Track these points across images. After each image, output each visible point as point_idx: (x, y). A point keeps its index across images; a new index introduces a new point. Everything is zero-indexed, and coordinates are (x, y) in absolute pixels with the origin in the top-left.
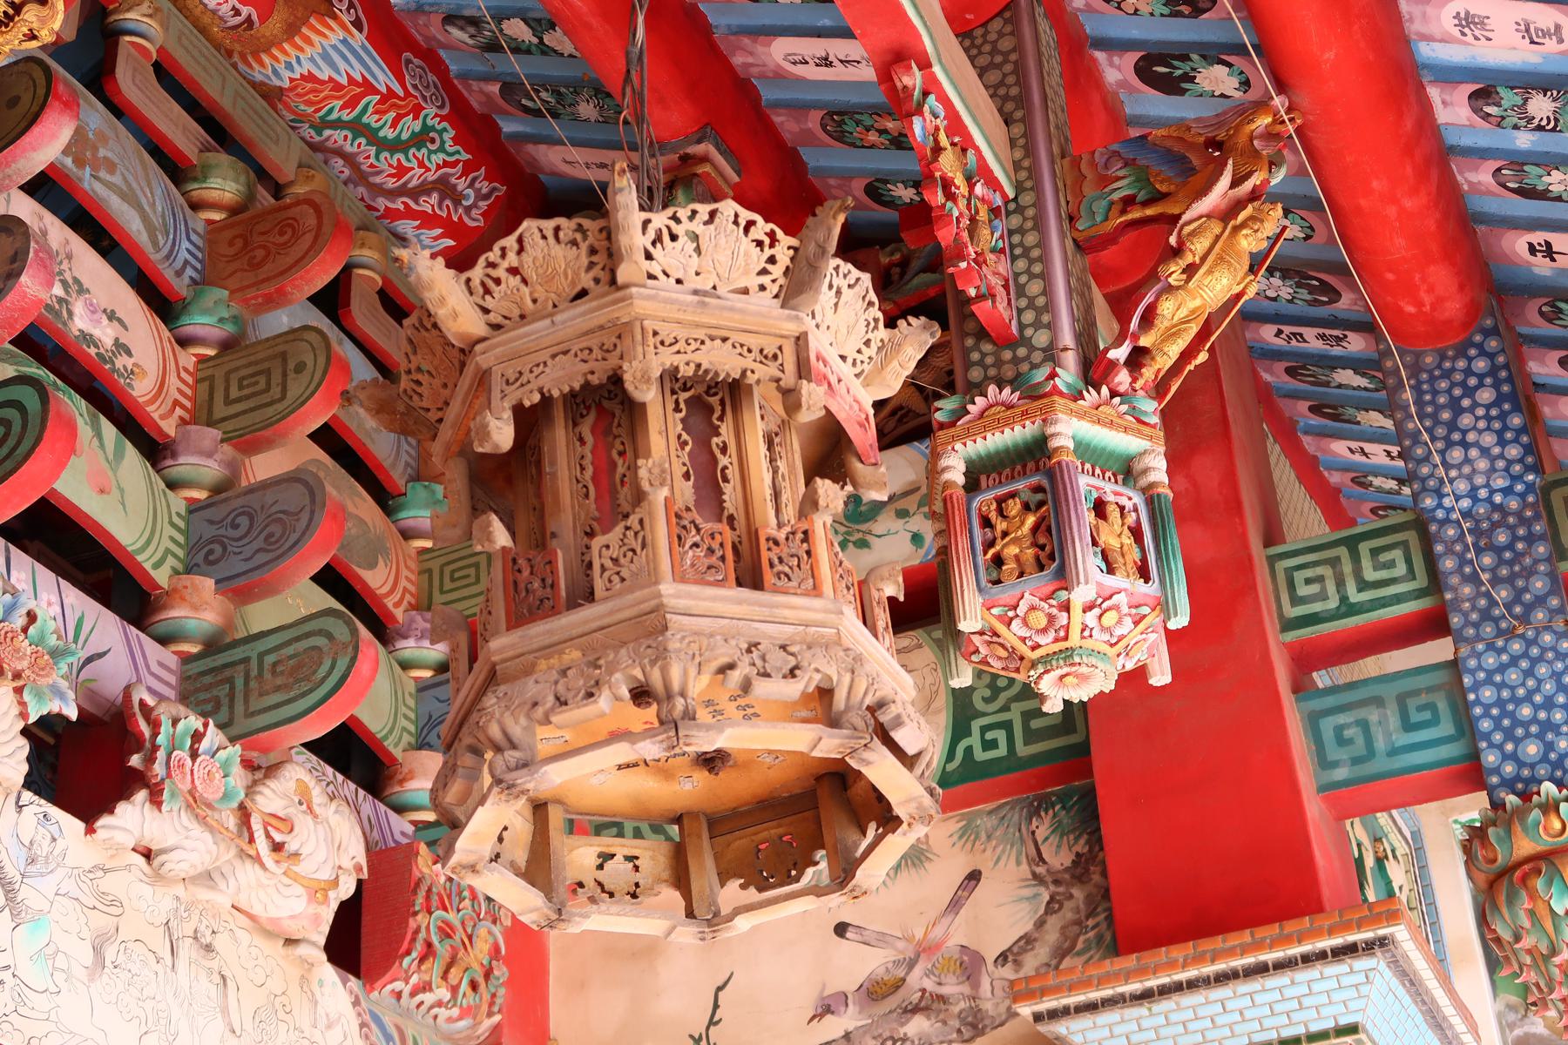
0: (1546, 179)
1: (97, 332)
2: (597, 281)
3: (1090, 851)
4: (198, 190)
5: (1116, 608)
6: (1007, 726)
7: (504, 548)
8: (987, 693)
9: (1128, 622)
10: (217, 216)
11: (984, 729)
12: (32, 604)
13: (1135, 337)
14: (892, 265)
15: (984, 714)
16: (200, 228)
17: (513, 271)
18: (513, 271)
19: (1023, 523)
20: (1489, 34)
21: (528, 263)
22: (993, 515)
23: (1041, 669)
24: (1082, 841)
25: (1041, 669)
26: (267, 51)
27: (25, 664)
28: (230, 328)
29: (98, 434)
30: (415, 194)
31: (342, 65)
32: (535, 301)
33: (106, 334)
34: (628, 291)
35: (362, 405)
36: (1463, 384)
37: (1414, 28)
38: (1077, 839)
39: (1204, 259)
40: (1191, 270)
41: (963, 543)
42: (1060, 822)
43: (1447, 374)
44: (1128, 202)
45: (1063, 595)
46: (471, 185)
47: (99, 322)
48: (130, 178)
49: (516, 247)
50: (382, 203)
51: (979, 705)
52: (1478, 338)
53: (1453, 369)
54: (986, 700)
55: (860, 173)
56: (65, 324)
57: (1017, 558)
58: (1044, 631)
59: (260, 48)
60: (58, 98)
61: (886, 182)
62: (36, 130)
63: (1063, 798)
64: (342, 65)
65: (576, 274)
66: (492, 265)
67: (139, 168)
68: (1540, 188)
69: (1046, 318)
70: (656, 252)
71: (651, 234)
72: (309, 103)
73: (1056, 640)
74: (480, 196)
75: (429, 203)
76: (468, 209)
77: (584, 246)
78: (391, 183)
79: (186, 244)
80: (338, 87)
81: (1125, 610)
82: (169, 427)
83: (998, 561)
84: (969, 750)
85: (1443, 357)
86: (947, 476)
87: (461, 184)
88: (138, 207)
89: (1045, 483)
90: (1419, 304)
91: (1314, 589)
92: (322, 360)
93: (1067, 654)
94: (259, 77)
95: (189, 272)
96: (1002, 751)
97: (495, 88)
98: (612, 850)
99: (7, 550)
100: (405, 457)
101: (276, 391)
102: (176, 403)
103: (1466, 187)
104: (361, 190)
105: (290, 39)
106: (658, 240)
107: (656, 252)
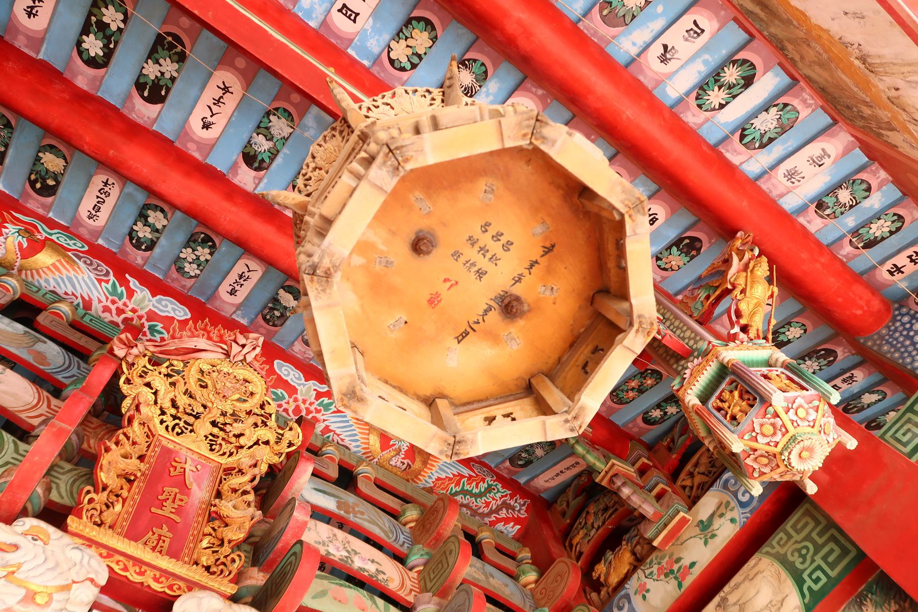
0: (871, 232)
1: (367, 567)
3: (900, 606)
4: (403, 519)
5: (800, 406)
6: (819, 568)
8: (801, 560)
9: (812, 411)
10: (412, 524)
11: (810, 576)
13: (738, 322)
14: (668, 444)
15: (805, 569)
16: (408, 530)
17: (315, 169)
18: (315, 169)
19: (733, 397)
20: (801, 175)
21: (319, 162)
22: (720, 404)
23: (786, 454)
24: (893, 604)
25: (786, 454)
26: (420, 474)
28: (426, 557)
29: (375, 603)
30: (497, 511)
31: (448, 471)
33: (371, 568)
36: (905, 329)
37: (774, 194)
38: (889, 604)
39: (746, 285)
40: (743, 291)
41: (713, 420)
42: (875, 601)
43: (896, 330)
44: (708, 297)
45: (770, 409)
46: (516, 502)
50: (487, 520)
51: (801, 567)
52: (897, 313)
53: (896, 328)
54: (802, 563)
55: (638, 415)
57: (741, 411)
58: (774, 434)
59: (418, 474)
60: (302, 457)
61: (647, 413)
63: (869, 590)
64: (448, 471)
68: (872, 238)
69: (698, 338)
70: (370, 114)
72: (443, 489)
73: (783, 435)
74: (521, 505)
75: (503, 513)
76: (519, 511)
77: (337, 134)
78: (486, 510)
79: (402, 536)
80: (450, 479)
81: (806, 406)
82: (410, 599)
83: (734, 418)
84: (809, 588)
85: (889, 327)
86: (691, 404)
87: (512, 502)
88: (378, 525)
89: (733, 377)
90: (861, 308)
91: (909, 435)
92: (457, 544)
93: (793, 439)
94: (422, 486)
95: (406, 545)
96: (824, 580)
97: (508, 464)
98: (492, 414)
100: (528, 604)
101: (445, 566)
102: (411, 590)
103: (845, 260)
104: (477, 518)
105: (426, 467)
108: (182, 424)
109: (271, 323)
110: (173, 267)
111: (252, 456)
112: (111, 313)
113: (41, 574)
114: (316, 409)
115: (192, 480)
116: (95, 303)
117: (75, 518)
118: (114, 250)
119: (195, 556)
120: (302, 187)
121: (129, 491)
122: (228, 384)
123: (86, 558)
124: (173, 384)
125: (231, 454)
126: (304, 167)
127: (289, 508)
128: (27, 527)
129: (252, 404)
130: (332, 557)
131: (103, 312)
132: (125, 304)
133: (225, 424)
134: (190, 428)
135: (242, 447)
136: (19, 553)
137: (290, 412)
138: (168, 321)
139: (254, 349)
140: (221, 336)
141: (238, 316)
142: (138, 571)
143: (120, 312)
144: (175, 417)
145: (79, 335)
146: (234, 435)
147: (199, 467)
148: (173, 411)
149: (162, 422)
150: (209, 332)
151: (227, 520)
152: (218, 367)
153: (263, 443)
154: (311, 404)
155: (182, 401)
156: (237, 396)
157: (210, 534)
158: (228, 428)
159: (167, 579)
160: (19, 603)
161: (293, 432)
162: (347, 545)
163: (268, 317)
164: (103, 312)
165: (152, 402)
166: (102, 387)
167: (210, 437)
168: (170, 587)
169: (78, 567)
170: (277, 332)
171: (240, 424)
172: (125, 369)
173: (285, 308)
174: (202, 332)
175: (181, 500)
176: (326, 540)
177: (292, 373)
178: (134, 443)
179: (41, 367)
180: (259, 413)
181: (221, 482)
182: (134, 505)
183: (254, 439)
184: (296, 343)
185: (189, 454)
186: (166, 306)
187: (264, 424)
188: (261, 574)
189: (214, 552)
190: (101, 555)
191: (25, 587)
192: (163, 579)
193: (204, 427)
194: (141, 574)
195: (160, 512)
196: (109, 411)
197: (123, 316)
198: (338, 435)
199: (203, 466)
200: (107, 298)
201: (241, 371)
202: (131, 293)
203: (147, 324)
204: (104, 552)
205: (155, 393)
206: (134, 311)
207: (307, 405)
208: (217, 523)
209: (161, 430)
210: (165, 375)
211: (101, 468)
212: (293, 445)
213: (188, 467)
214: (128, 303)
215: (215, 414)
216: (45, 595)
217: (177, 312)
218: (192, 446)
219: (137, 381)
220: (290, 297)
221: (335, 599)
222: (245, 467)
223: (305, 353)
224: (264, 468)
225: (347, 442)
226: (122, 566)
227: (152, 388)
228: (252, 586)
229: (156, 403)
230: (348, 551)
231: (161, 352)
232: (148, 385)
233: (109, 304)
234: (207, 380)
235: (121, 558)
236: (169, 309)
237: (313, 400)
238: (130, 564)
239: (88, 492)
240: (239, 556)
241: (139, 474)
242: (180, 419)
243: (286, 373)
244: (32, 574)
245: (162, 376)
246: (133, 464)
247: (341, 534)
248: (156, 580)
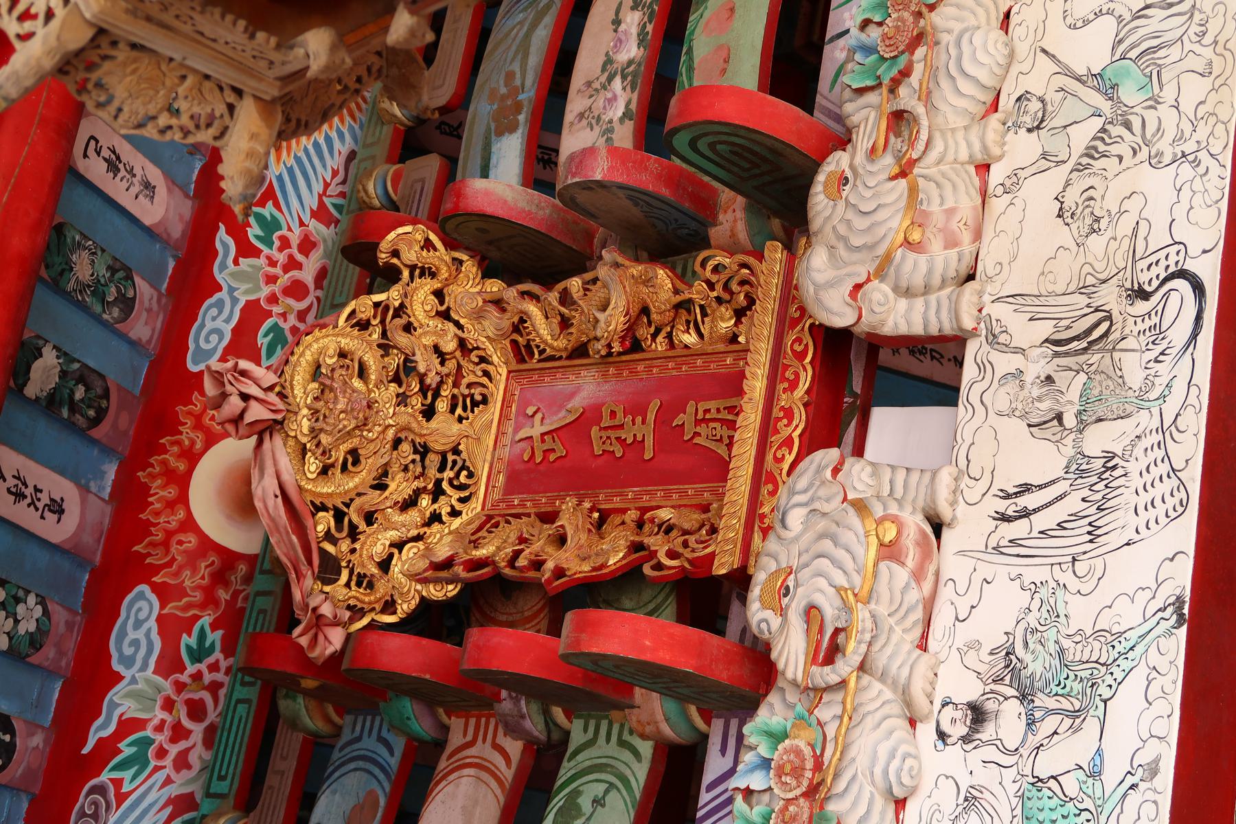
1: (634, 31)
2: (114, 44)
7: (412, 13)
12: (854, 32)
27: (906, 14)
32: (184, 77)
34: (94, 21)
35: (420, 100)
47: (625, 32)
48: (511, 54)
49: (150, 126)
56: (639, 65)
60: (457, 207)
62: (489, 210)
65: (125, 64)
66: (186, 133)
67: (500, 50)
70: (39, 8)
71: (28, 26)
77: (94, 76)
88: (528, 36)
99: (832, 40)
106: (26, 16)
107: (39, 8)
108: (449, 474)
109: (104, 404)
110: (35, 659)
111: (478, 315)
112: (188, 750)
113: (848, 551)
114: (281, 250)
115: (563, 413)
116: (174, 790)
117: (716, 563)
118: (25, 806)
119: (721, 347)
120: (212, 131)
121: (624, 511)
122: (340, 406)
123: (798, 499)
124: (369, 518)
125: (483, 360)
126: (168, 136)
127: (582, 197)
128: (768, 614)
129: (364, 348)
130: (633, 106)
131: (189, 767)
132: (159, 728)
133: (424, 390)
134: (450, 457)
135: (462, 343)
136: (819, 600)
137: (302, 305)
138: (170, 628)
139: (244, 373)
140: (171, 505)
141: (102, 488)
142: (785, 421)
143: (179, 733)
144: (438, 492)
145: (271, 780)
146: (442, 363)
147: (530, 411)
148: (425, 501)
149: (455, 513)
150: (170, 534)
151: (634, 312)
152: (304, 440)
153: (442, 303)
154: (272, 263)
155: (400, 487)
156: (357, 383)
157: (669, 336)
158: (432, 380)
159: (786, 367)
160: (903, 564)
161: (403, 248)
162: (597, 85)
163: (91, 413)
164: (189, 767)
165: (421, 545)
166: (425, 642)
167: (459, 411)
168: (801, 356)
169: (817, 505)
170: (120, 388)
171: (418, 357)
172: (365, 621)
173: (64, 374)
174: (174, 548)
175: (613, 414)
176: (597, 129)
177: (210, 325)
178: (522, 540)
179: (382, 802)
180: (379, 330)
181: (552, 358)
182: (648, 493)
183: (438, 323)
184: (133, 335)
185: (507, 440)
186: (135, 643)
187: (400, 311)
188: (721, 217)
189: (704, 314)
190: (773, 493)
191: (876, 565)
192: (789, 374)
193: (443, 429)
194: (789, 414)
195: (649, 442)
196: (484, 595)
197: (186, 723)
198: (327, 185)
199: (524, 404)
200: (157, 769)
201: (298, 391)
202: (128, 726)
203: (191, 669)
204: (766, 489)
205: (399, 545)
206: (168, 705)
207: (278, 271)
208: (644, 332)
209: (476, 506)
210: (354, 540)
211: (603, 566)
212: (427, 240)
213: (536, 430)
214: (156, 722)
215: (410, 414)
216: (880, 529)
217: (142, 616)
218: (486, 440)
219: (382, 589)
220: (37, 366)
221: (724, 71)
222: (506, 322)
223: (149, 310)
224: (494, 286)
225: (336, 162)
226: (785, 450)
227: (391, 556)
228: (749, 225)
229: (418, 538)
230: (610, 79)
231: (310, 563)
232: (385, 565)
233: (168, 761)
234: (339, 455)
235: (769, 457)
236: (140, 635)
237: (262, 261)
238: (776, 440)
239: (659, 566)
240: (703, 264)
241: (587, 505)
242: (438, 482)
243: (214, 338)
244: (849, 564)
245: (357, 546)
246: (572, 516)
247: (575, 104)
248: (794, 385)
